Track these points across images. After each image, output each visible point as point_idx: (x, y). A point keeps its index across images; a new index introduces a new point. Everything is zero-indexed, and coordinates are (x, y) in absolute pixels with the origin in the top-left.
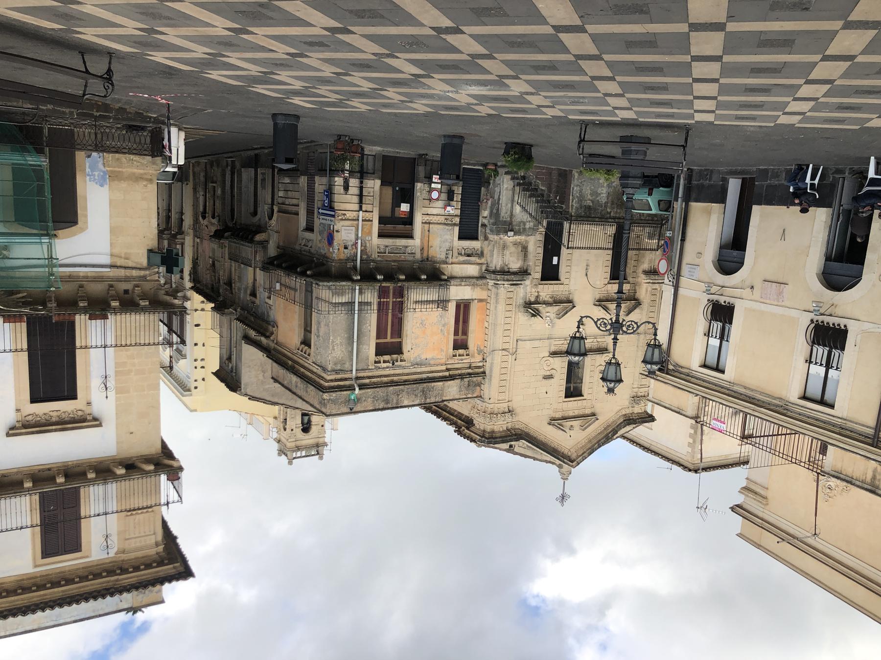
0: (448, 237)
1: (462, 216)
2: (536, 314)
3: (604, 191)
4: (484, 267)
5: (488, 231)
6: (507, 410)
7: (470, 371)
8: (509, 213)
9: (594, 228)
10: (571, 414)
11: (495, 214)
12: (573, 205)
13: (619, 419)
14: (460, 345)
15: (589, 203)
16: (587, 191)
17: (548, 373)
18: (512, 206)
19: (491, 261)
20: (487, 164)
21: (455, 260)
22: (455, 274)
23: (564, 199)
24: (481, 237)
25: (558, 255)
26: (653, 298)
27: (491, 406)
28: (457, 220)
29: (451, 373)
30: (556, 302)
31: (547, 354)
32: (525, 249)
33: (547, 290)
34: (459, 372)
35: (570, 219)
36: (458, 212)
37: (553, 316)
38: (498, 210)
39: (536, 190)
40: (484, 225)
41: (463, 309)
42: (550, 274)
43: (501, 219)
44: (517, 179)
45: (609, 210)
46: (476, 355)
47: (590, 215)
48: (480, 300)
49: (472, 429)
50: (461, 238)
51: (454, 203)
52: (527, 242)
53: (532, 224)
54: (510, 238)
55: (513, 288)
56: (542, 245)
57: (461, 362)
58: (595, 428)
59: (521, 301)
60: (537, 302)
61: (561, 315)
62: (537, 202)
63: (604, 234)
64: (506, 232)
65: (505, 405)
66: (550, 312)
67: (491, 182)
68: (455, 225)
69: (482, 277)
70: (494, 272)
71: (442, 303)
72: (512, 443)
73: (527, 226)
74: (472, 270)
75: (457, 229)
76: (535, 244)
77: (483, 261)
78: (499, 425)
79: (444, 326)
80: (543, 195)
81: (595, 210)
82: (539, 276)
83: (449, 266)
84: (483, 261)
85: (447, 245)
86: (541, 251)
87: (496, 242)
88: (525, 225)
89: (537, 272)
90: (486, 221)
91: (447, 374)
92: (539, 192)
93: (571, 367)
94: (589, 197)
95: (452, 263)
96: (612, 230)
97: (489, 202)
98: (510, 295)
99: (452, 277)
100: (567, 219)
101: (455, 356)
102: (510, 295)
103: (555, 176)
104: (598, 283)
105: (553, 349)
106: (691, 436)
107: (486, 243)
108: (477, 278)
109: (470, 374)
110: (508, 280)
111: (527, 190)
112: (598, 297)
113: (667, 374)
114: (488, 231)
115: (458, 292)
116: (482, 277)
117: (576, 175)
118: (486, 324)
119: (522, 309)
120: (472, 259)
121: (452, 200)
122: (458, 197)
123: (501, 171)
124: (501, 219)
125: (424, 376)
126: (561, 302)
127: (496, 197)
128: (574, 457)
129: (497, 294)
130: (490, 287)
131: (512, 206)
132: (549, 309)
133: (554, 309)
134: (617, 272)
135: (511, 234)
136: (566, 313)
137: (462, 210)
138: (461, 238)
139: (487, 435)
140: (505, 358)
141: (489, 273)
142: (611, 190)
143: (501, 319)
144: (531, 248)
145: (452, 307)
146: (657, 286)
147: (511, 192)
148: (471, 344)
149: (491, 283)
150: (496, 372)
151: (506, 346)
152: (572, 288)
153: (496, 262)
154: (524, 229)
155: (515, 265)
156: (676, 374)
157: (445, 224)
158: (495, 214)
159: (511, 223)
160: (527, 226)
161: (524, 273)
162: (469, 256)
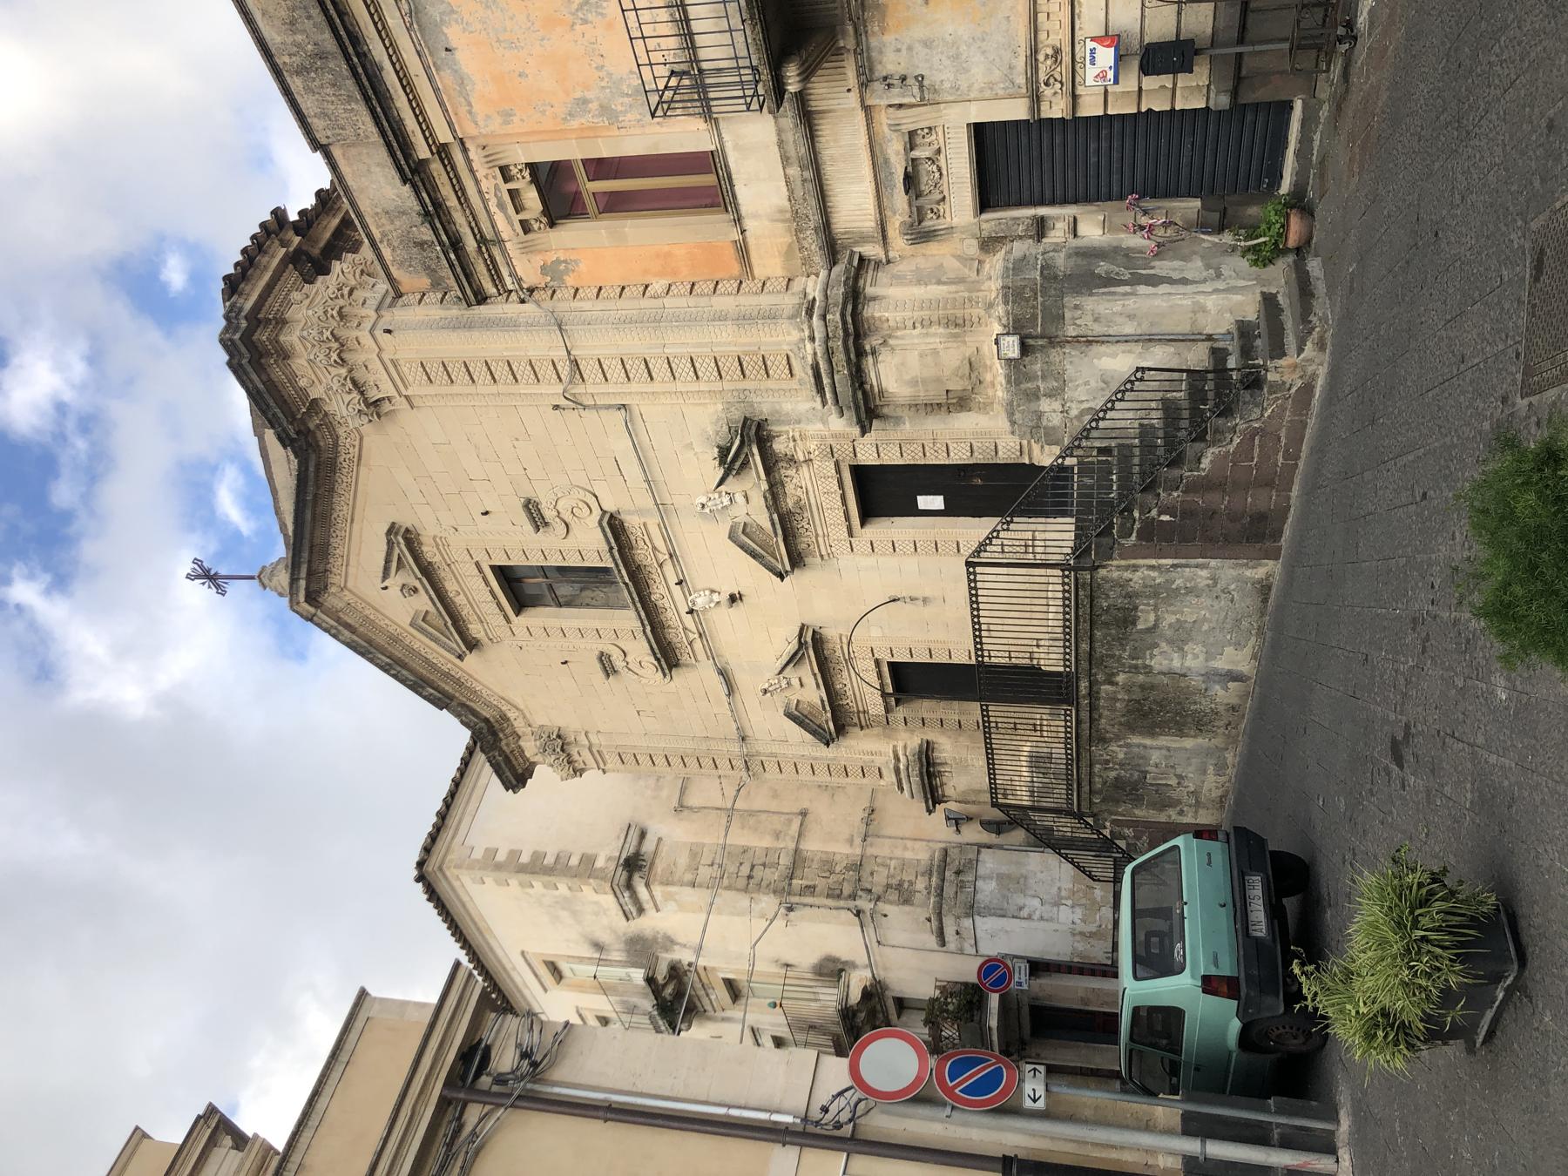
0: (978, 73)
1: (1075, 125)
2: (731, 463)
3: (1190, 662)
4: (872, 250)
5: (1020, 248)
6: (374, 395)
7: (470, 244)
8: (1098, 329)
9: (1056, 608)
10: (451, 587)
11: (1090, 273)
12: (1131, 571)
13: (488, 705)
14: (558, 192)
15: (1146, 619)
16: (1189, 611)
17: (549, 514)
18: (1126, 339)
19: (899, 280)
20: (1307, 211)
21: (883, 119)
22: (825, 129)
23: (1156, 538)
24: (995, 219)
25: (949, 511)
26: (854, 770)
27: (367, 340)
28: (1055, 108)
29: (436, 168)
30: (787, 523)
31: (610, 507)
32: (959, 402)
33: (821, 492)
34: (452, 202)
35: (1082, 563)
36: (1091, 107)
37: (740, 512)
38: (1109, 281)
39: (1201, 438)
40: (1041, 228)
41: (701, 185)
42: (880, 492)
43: (1070, 301)
44: (1246, 352)
45: (1121, 678)
46: (538, 260)
47: (1096, 617)
48: (743, 251)
49: (292, 275)
50: (981, 133)
51: (1130, 82)
52: (985, 408)
53: (1056, 420)
54: (993, 342)
55: (804, 373)
56: (979, 458)
57: (495, 208)
58: (439, 655)
59: (764, 407)
60: (771, 464)
61: (743, 537)
62: (1145, 431)
63: (1031, 629)
64: (1016, 326)
65: (387, 389)
66: (748, 500)
67: (1227, 238)
68: (1036, 98)
69: (832, 248)
70: (855, 297)
71: (692, 87)
72: (1042, 211)
73: (1046, 405)
74: (854, 205)
75: (1017, 111)
76: (984, 434)
77: (898, 243)
78: (311, 372)
79: (605, 110)
80: (1176, 462)
81: (1122, 641)
82: (867, 457)
83: (853, 100)
84: (898, 243)
85: (941, 74)
86: (960, 456)
87: (974, 287)
88: (1051, 395)
89: (880, 449)
90: (1058, 234)
91: (423, 152)
92: (1191, 449)
93: (594, 576)
94: (1172, 619)
95: (867, 109)
96: (1051, 660)
97: (1136, 241)
98: (778, 367)
99: (808, 119)
100: (1081, 550)
101: (507, 178)
102: (778, 367)
103: (1255, 501)
104: (875, 632)
105: (632, 522)
106: (514, 854)
107: (972, 247)
108: (826, 226)
109: (456, 244)
110: (829, 354)
111: (1196, 395)
112: (831, 633)
113: (444, 1103)
114: (1020, 248)
115: (754, 146)
116: (832, 248)
117: (1259, 572)
118: (658, 286)
119: (737, 415)
120: (899, 200)
121: (1147, 68)
122: (1158, 93)
123: (1278, 276)
124: (1070, 301)
125: (378, 51)
126: (789, 536)
127: (1162, 267)
128: (331, 600)
129: (771, 316)
130: (797, 286)
131: (1126, 339)
132: (758, 501)
133: (761, 517)
134: (909, 681)
135: (1011, 347)
136: (754, 555)
137: (1105, 121)
138: (981, 133)
139: (262, 336)
140: (546, 372)
141: (851, 275)
142: (1196, 682)
143: (681, 343)
144: (965, 423)
145: (684, 134)
146: (890, 777)
147: (1184, 328)
148: (572, 237)
149: (814, 288)
150: (493, 345)
151: (589, 369)
152: (845, 560)
153: (894, 299)
154: (1034, 396)
155: (891, 374)
156: (439, 1150)
157: (1034, 51)
158: (1090, 273)
159: (1053, 341)
160: (1046, 405)
161: (869, 410)
162: (911, 181)
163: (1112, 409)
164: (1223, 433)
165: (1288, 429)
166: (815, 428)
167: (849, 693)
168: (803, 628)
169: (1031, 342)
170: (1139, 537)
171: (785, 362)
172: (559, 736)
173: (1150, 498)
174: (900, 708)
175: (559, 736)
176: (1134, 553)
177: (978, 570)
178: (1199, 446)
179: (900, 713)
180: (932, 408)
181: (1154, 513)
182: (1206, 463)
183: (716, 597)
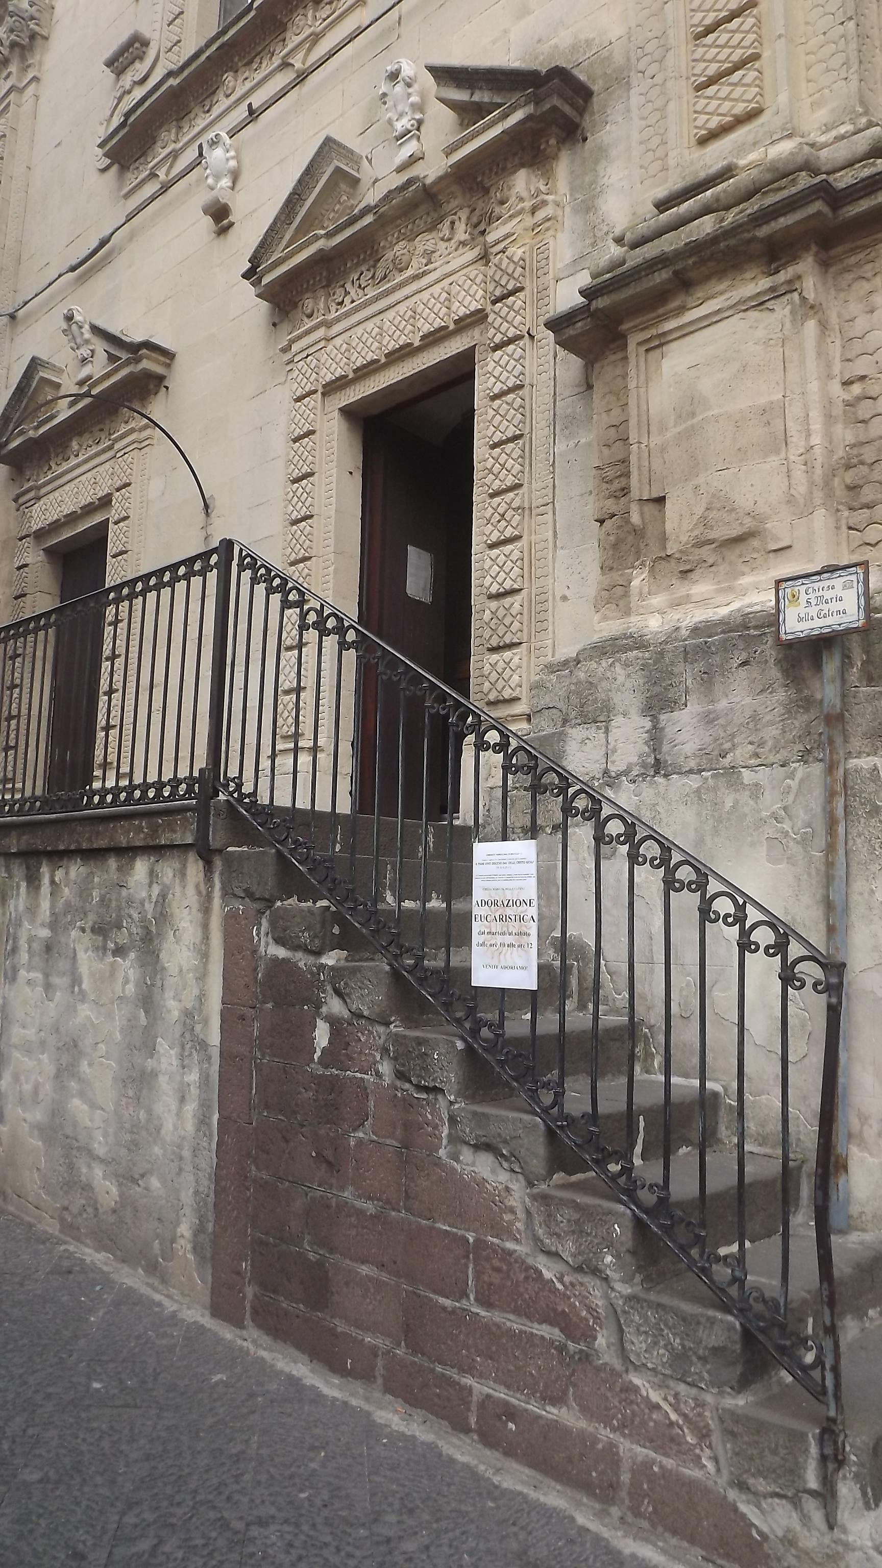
23: (267, 1006)
32: (631, 532)
52: (615, 596)
56: (483, 612)
163: (670, 884)
164: (578, 1231)
165: (586, 1441)
166: (563, 247)
167: (66, 466)
168: (168, 355)
169: (831, 666)
170: (276, 962)
171: (740, 109)
172: (33, 36)
173: (371, 995)
174: (41, 556)
175: (33, 36)
176: (238, 949)
177: (213, 577)
178: (536, 1149)
179: (33, 556)
180: (615, 477)
181: (335, 1006)
182: (482, 1167)
183: (225, 182)
